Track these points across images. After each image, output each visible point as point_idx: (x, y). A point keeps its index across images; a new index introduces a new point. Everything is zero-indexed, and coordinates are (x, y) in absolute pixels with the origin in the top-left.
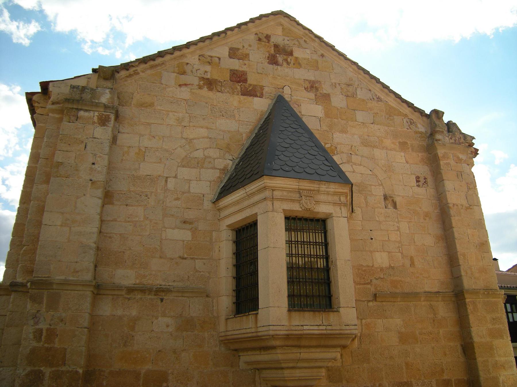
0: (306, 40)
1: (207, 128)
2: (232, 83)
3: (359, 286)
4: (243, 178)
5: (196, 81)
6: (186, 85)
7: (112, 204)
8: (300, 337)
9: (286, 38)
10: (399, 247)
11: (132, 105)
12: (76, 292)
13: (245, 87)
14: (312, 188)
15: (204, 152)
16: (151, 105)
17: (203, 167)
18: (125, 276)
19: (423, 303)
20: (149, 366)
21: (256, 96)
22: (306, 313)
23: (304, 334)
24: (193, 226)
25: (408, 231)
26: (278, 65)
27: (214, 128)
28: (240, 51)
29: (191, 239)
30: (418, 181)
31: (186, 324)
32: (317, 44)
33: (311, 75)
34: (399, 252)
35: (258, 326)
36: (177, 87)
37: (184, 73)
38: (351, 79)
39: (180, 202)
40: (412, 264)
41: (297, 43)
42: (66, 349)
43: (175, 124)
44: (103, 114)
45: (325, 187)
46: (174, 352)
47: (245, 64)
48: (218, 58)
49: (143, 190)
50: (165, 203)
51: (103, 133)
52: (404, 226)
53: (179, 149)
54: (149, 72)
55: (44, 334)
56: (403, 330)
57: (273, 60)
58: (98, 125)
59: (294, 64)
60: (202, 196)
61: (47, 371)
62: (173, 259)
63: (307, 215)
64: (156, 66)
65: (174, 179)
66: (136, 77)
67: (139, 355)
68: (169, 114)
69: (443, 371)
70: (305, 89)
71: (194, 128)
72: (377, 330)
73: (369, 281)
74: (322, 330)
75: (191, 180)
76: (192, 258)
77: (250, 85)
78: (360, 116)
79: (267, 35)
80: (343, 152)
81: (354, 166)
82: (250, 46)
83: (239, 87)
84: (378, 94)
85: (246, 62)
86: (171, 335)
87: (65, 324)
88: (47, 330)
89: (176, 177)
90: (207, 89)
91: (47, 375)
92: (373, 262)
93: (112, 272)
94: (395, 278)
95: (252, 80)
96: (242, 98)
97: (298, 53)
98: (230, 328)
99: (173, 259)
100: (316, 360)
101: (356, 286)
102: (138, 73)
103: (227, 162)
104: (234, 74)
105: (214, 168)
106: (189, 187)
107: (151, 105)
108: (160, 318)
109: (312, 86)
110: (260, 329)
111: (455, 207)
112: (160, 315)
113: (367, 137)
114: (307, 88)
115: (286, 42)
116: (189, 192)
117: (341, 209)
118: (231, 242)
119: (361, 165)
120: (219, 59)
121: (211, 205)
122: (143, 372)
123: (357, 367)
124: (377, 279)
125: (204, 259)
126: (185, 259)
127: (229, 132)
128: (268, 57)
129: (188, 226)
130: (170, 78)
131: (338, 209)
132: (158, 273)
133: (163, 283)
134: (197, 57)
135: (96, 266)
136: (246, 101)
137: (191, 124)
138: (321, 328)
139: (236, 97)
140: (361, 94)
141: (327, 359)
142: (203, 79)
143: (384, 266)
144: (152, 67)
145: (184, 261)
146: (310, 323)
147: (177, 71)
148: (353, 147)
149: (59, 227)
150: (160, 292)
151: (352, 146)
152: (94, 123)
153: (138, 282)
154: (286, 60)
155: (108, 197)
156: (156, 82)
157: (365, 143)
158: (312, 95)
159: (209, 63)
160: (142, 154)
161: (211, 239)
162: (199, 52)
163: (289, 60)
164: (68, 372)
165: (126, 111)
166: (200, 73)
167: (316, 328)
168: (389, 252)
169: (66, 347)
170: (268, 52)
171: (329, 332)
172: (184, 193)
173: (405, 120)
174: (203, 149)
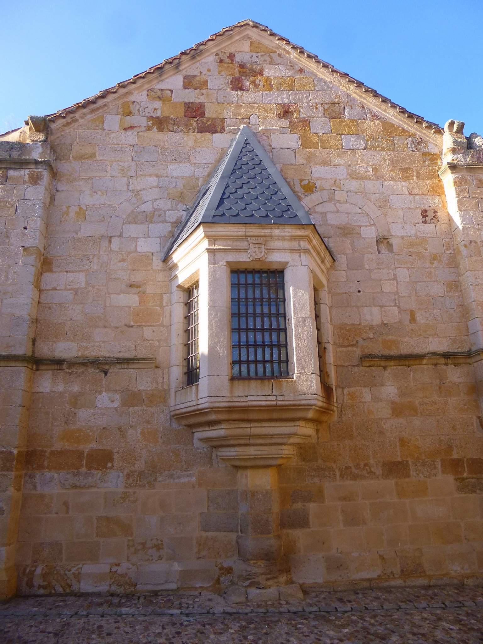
1: (157, 176)
2: (186, 119)
3: (341, 349)
5: (143, 121)
6: (131, 128)
7: (51, 271)
8: (246, 410)
9: (254, 54)
10: (395, 300)
11: (71, 158)
12: (9, 368)
14: (262, 234)
15: (153, 204)
17: (151, 222)
18: (65, 349)
19: (426, 367)
20: (93, 446)
21: (216, 131)
22: (252, 381)
23: (249, 406)
24: (141, 289)
25: (408, 280)
26: (243, 90)
27: (165, 175)
28: (197, 79)
29: (138, 305)
30: (424, 216)
31: (132, 399)
33: (285, 98)
34: (395, 305)
35: (199, 398)
37: (130, 114)
39: (126, 263)
40: (413, 319)
41: (268, 59)
43: (120, 175)
44: (35, 172)
45: (279, 230)
46: (120, 429)
47: (203, 94)
48: (170, 90)
50: (108, 266)
51: (36, 194)
52: (403, 274)
53: (125, 203)
54: (89, 117)
56: (398, 400)
57: (237, 85)
58: (30, 185)
59: (264, 86)
60: (151, 255)
62: (118, 328)
63: (258, 267)
64: (98, 109)
65: (119, 239)
66: (76, 125)
67: (82, 434)
69: (450, 448)
72: (363, 400)
73: (354, 342)
74: (270, 401)
75: (137, 238)
76: (139, 326)
77: (209, 119)
79: (231, 54)
80: (324, 189)
81: (338, 205)
82: (209, 70)
83: (194, 123)
85: (203, 91)
86: (117, 410)
89: (121, 236)
90: (156, 130)
92: (360, 320)
93: (52, 345)
94: (390, 337)
95: (210, 112)
96: (199, 135)
97: (270, 72)
99: (118, 328)
100: (272, 436)
101: (338, 349)
102: (77, 120)
104: (189, 108)
106: (136, 246)
107: (93, 155)
108: (104, 394)
109: (286, 112)
110: (200, 402)
111: (473, 244)
112: (104, 389)
114: (280, 114)
115: (255, 59)
116: (136, 251)
117: (300, 256)
118: (182, 305)
119: (347, 202)
121: (161, 264)
123: (336, 443)
125: (154, 326)
126: (132, 326)
127: (182, 177)
128: (232, 82)
129: (134, 290)
130: (113, 121)
131: (296, 256)
132: (104, 345)
134: (145, 93)
135: (34, 341)
136: (203, 138)
138: (270, 398)
139: (192, 136)
141: (285, 435)
142: (152, 118)
143: (374, 323)
144: (92, 111)
145: (131, 329)
146: (256, 394)
148: (337, 182)
151: (335, 181)
152: (25, 182)
153: (80, 354)
154: (254, 82)
155: (46, 264)
156: (97, 128)
158: (285, 123)
159: (159, 97)
160: (82, 213)
161: (161, 303)
162: (147, 86)
165: (64, 167)
166: (149, 112)
167: (263, 398)
168: (382, 307)
170: (232, 75)
171: (280, 403)
172: (129, 253)
174: (152, 200)
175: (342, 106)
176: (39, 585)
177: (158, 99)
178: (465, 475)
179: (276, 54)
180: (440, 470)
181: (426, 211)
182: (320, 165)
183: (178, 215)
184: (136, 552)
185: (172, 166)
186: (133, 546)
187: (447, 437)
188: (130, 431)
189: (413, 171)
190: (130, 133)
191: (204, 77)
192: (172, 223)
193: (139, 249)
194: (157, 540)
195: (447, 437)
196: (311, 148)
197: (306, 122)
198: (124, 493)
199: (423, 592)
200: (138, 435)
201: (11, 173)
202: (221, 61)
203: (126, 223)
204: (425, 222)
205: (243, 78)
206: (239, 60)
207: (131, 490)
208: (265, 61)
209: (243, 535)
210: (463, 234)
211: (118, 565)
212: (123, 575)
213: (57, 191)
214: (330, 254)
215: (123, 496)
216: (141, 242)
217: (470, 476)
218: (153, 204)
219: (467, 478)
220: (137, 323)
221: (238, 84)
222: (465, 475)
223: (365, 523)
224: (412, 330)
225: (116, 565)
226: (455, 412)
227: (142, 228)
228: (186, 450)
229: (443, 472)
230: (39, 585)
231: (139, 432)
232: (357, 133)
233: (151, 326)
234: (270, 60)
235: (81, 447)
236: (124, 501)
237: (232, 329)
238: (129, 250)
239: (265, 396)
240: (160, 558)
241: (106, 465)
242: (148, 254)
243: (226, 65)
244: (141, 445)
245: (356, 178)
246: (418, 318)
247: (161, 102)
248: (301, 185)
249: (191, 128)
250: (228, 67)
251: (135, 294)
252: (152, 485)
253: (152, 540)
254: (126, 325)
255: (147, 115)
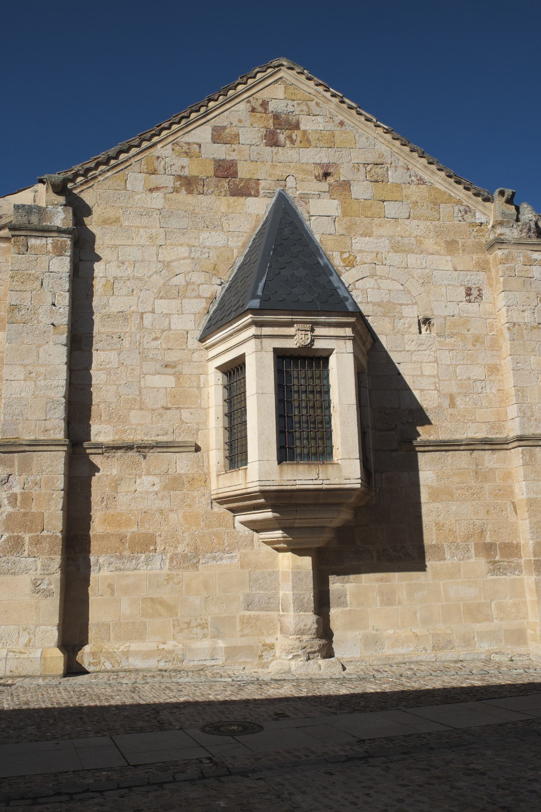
0: (319, 101)
4: (230, 311)
5: (169, 181)
6: (157, 189)
13: (235, 184)
15: (185, 277)
16: (117, 220)
17: (185, 297)
20: (135, 529)
21: (250, 195)
24: (177, 369)
26: (279, 146)
28: (227, 131)
29: (174, 386)
30: (468, 295)
31: (175, 483)
32: (332, 106)
33: (324, 156)
35: (248, 482)
36: (148, 193)
37: (154, 172)
38: (381, 156)
40: (453, 404)
41: (305, 108)
42: (43, 514)
43: (147, 243)
44: (59, 241)
47: (234, 150)
48: (198, 144)
49: (116, 331)
55: (19, 498)
57: (272, 141)
59: (301, 142)
60: (185, 333)
61: (27, 537)
62: (155, 410)
65: (151, 315)
68: (139, 232)
70: (316, 177)
71: (172, 247)
75: (171, 314)
76: (177, 408)
77: (242, 180)
78: (391, 209)
79: (264, 101)
81: (379, 281)
82: (240, 121)
83: (226, 185)
84: (420, 173)
87: (40, 487)
88: (22, 494)
90: (185, 192)
91: (27, 539)
95: (244, 171)
96: (232, 199)
97: (306, 124)
98: (221, 486)
103: (216, 289)
104: (220, 166)
105: (199, 297)
106: (170, 323)
107: (117, 220)
108: (144, 477)
110: (249, 485)
113: (400, 239)
114: (319, 175)
116: (170, 329)
118: (221, 387)
119: (387, 278)
120: (200, 146)
122: (129, 535)
124: (404, 424)
125: (191, 408)
126: (169, 409)
127: (215, 248)
128: (266, 136)
129: (170, 370)
133: (146, 438)
137: (168, 242)
140: (393, 176)
142: (180, 177)
145: (169, 411)
147: (146, 171)
149: (23, 382)
150: (142, 448)
151: (377, 254)
152: (48, 253)
154: (290, 137)
157: (396, 248)
158: (324, 186)
159: (186, 153)
163: (294, 137)
164: (48, 536)
166: (176, 170)
169: (43, 511)
173: (456, 208)
175: (386, 167)
176: (90, 662)
177: (185, 155)
178: (497, 558)
179: (314, 102)
180: (473, 554)
181: (469, 289)
182: (361, 235)
183: (212, 289)
184: (181, 631)
185: (204, 235)
186: (178, 625)
187: (481, 522)
188: (171, 515)
189: (458, 245)
190: (157, 194)
191: (234, 130)
192: (206, 298)
193: (173, 327)
194: (201, 619)
195: (481, 522)
196: (352, 216)
197: (346, 185)
198: (168, 575)
199: (452, 665)
200: (180, 518)
201: (32, 242)
202: (253, 110)
203: (157, 299)
204: (470, 301)
205: (278, 131)
206: (273, 109)
207: (174, 572)
208: (302, 111)
209: (285, 613)
210: (507, 316)
211: (164, 643)
212: (170, 652)
213: (80, 260)
214: (372, 336)
215: (167, 578)
216: (175, 319)
217: (502, 560)
218: (185, 277)
219: (499, 562)
220: (174, 405)
221: (273, 138)
222: (497, 558)
223: (400, 603)
224: (451, 414)
225: (163, 643)
226: (490, 497)
227: (174, 304)
228: (228, 533)
229: (476, 555)
230: (90, 662)
231: (180, 516)
232: (400, 199)
233: (189, 408)
234: (307, 110)
235: (124, 530)
236: (168, 583)
237: (280, 415)
238: (162, 328)
239: (312, 480)
240: (205, 636)
241: (149, 548)
242: (182, 332)
243: (258, 115)
244: (183, 529)
245: (399, 252)
246: (458, 403)
247: (188, 159)
248: (341, 259)
249: (222, 190)
250: (261, 117)
251: (171, 374)
252: (195, 566)
253: (196, 619)
254: (163, 407)
255: (174, 174)
